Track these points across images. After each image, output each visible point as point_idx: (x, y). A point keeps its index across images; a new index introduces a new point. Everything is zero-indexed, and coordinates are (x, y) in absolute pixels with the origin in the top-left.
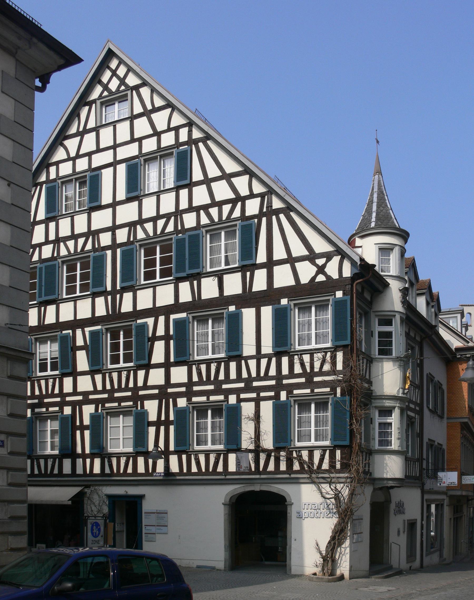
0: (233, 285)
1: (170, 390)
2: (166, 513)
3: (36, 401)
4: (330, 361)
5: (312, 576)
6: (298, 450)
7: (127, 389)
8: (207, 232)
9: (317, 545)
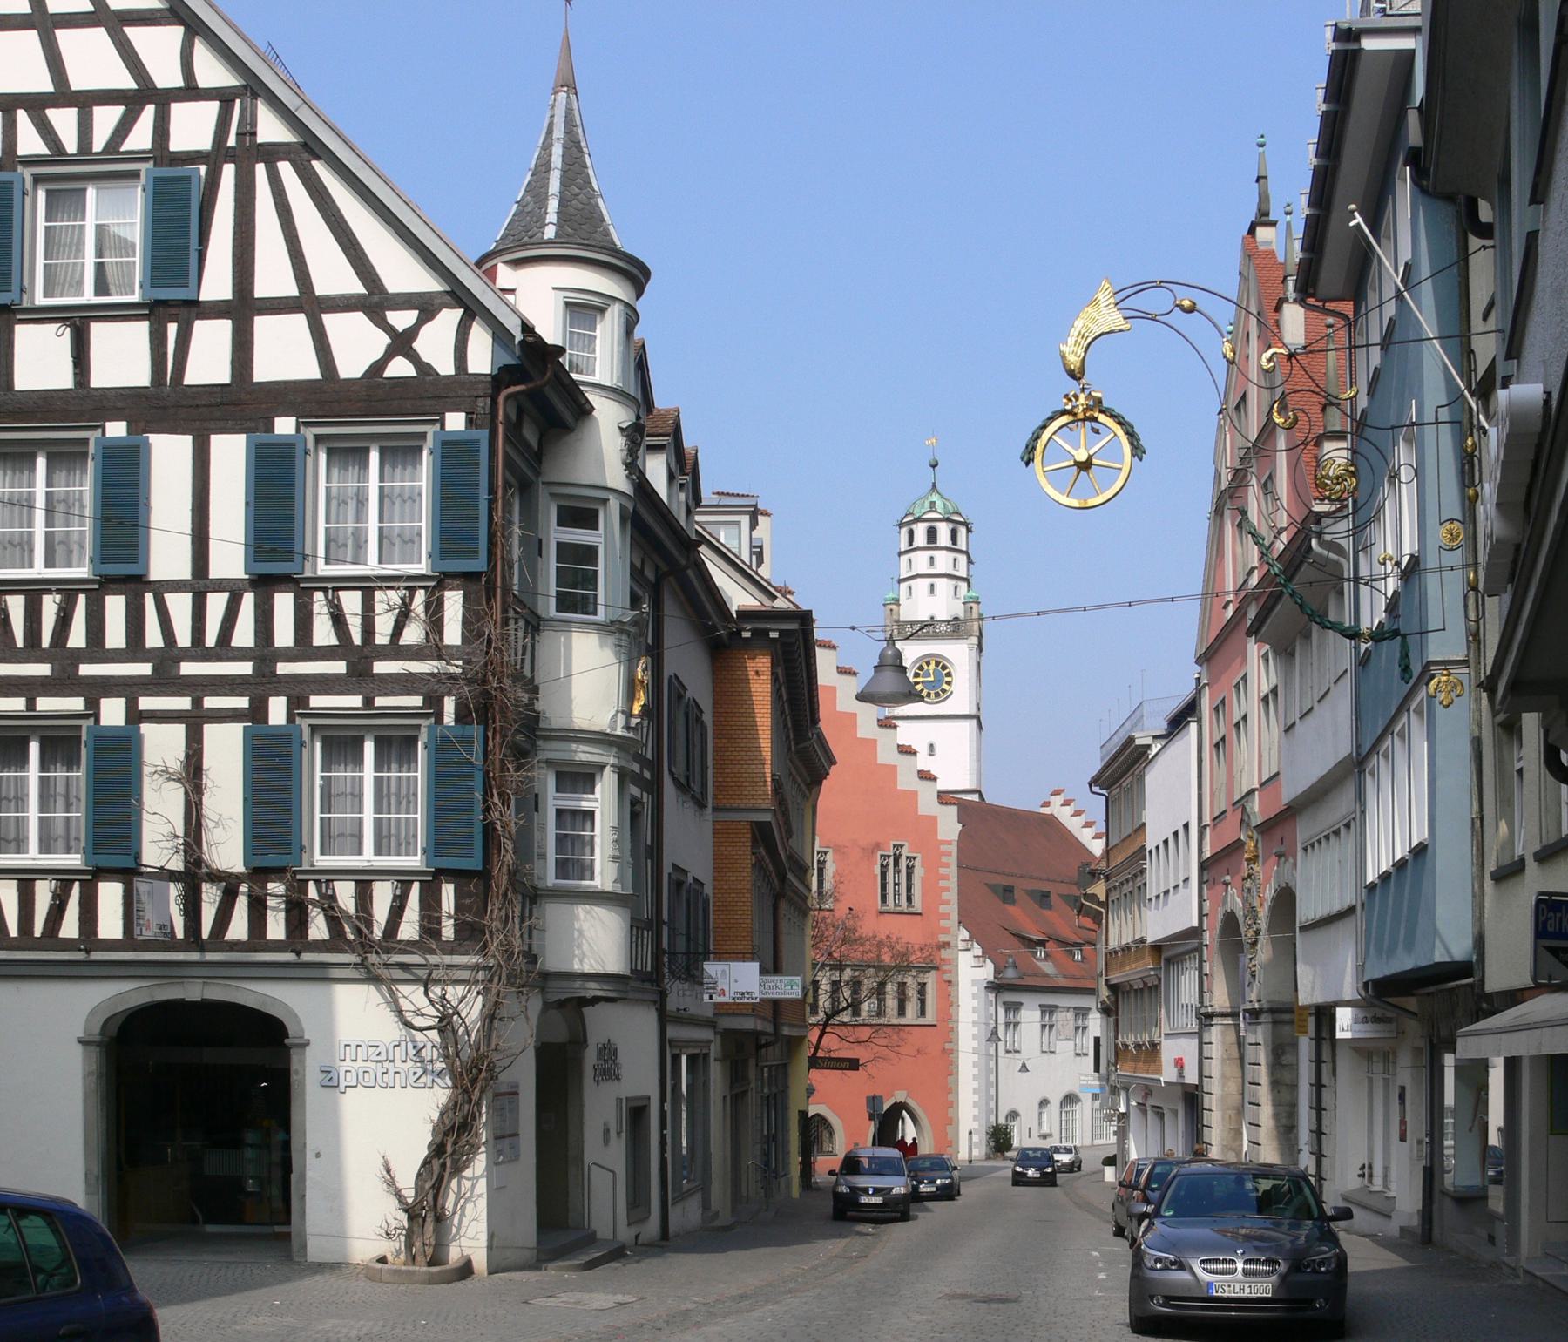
0: (122, 357)
4: (423, 616)
5: (379, 1266)
6: (323, 878)
8: (37, 180)
9: (388, 1171)
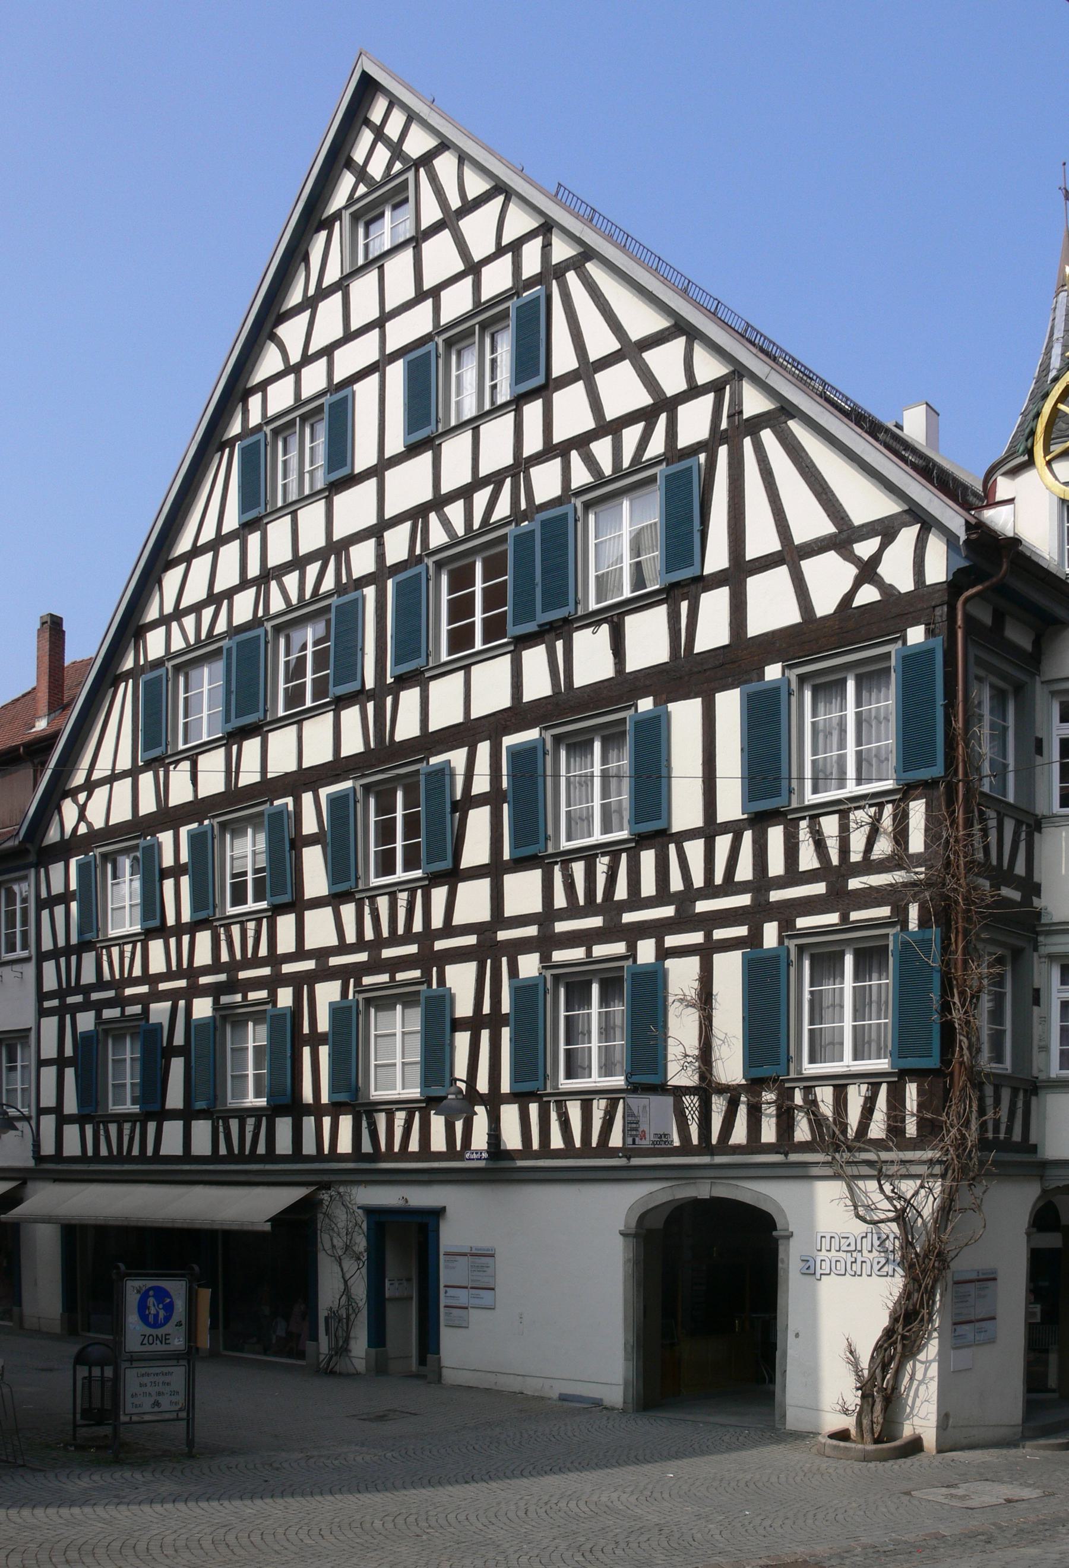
0: (648, 640)
1: (503, 935)
2: (493, 1256)
3: (222, 977)
7: (409, 937)
